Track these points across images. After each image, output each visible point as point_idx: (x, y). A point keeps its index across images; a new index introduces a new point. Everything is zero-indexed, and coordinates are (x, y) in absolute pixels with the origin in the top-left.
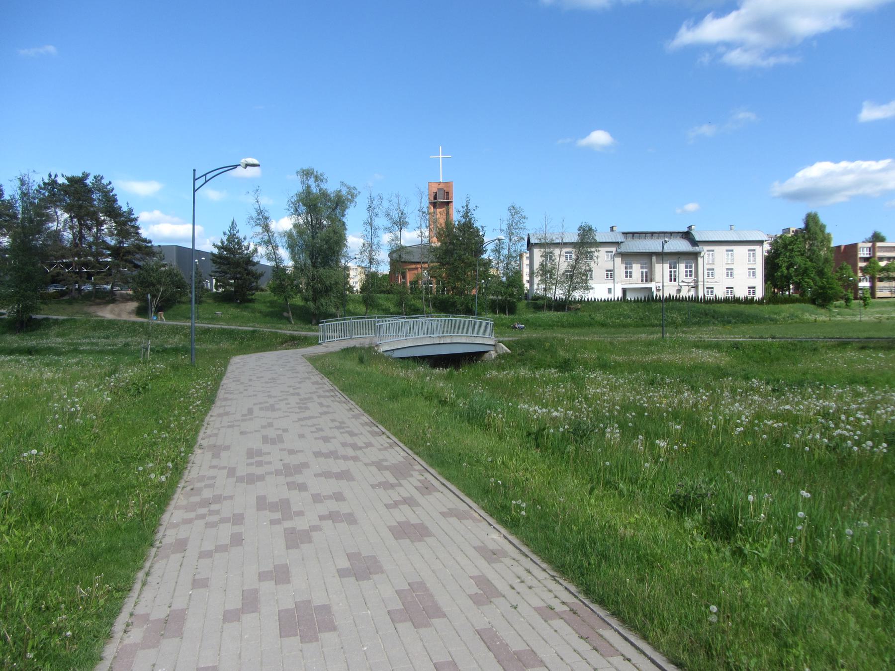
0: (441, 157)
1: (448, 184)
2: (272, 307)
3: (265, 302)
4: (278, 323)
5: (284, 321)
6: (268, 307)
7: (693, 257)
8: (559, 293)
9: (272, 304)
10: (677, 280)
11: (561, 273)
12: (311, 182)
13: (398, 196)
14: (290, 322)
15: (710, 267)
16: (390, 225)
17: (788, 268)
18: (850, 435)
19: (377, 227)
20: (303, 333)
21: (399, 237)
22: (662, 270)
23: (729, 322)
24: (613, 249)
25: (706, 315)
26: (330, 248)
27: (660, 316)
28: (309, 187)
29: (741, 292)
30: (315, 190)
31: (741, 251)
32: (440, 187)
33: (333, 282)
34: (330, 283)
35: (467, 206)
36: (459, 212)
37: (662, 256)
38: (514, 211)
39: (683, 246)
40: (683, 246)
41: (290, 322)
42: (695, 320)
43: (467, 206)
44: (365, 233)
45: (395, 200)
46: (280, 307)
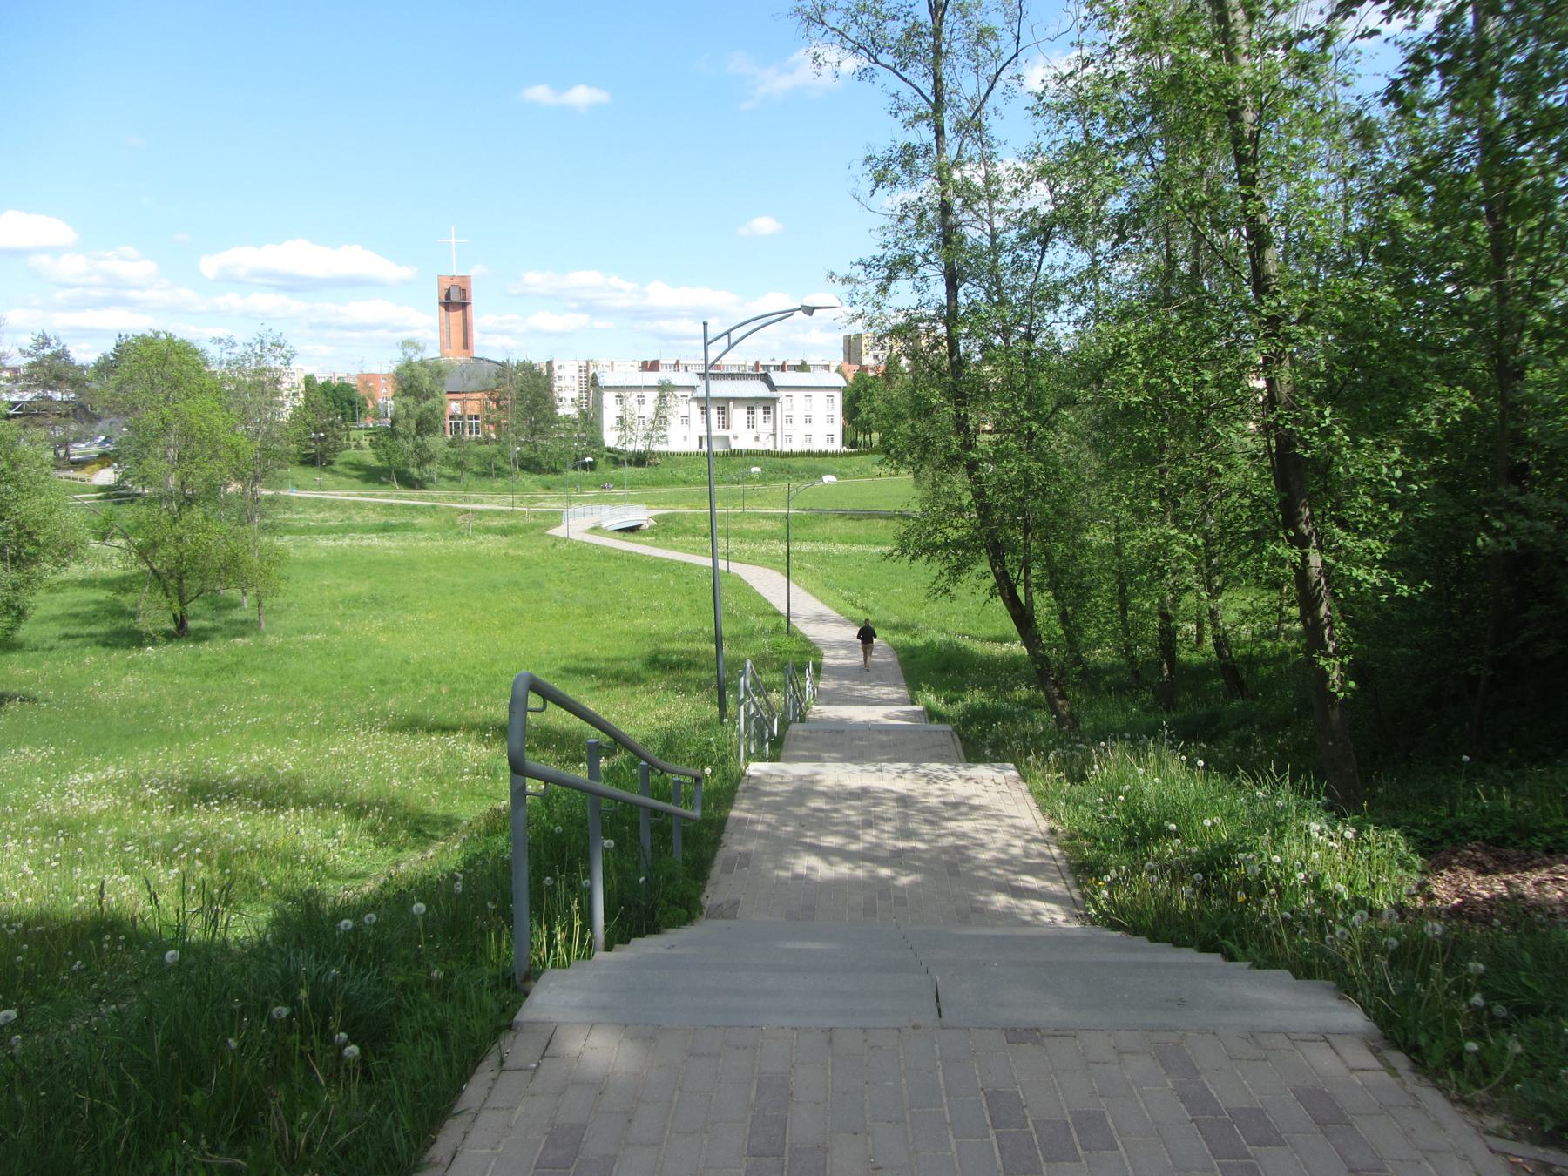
0: (453, 241)
1: (465, 279)
18: (1318, 265)
23: (803, 477)
24: (688, 393)
27: (739, 471)
39: (758, 389)
40: (758, 389)
42: (771, 475)
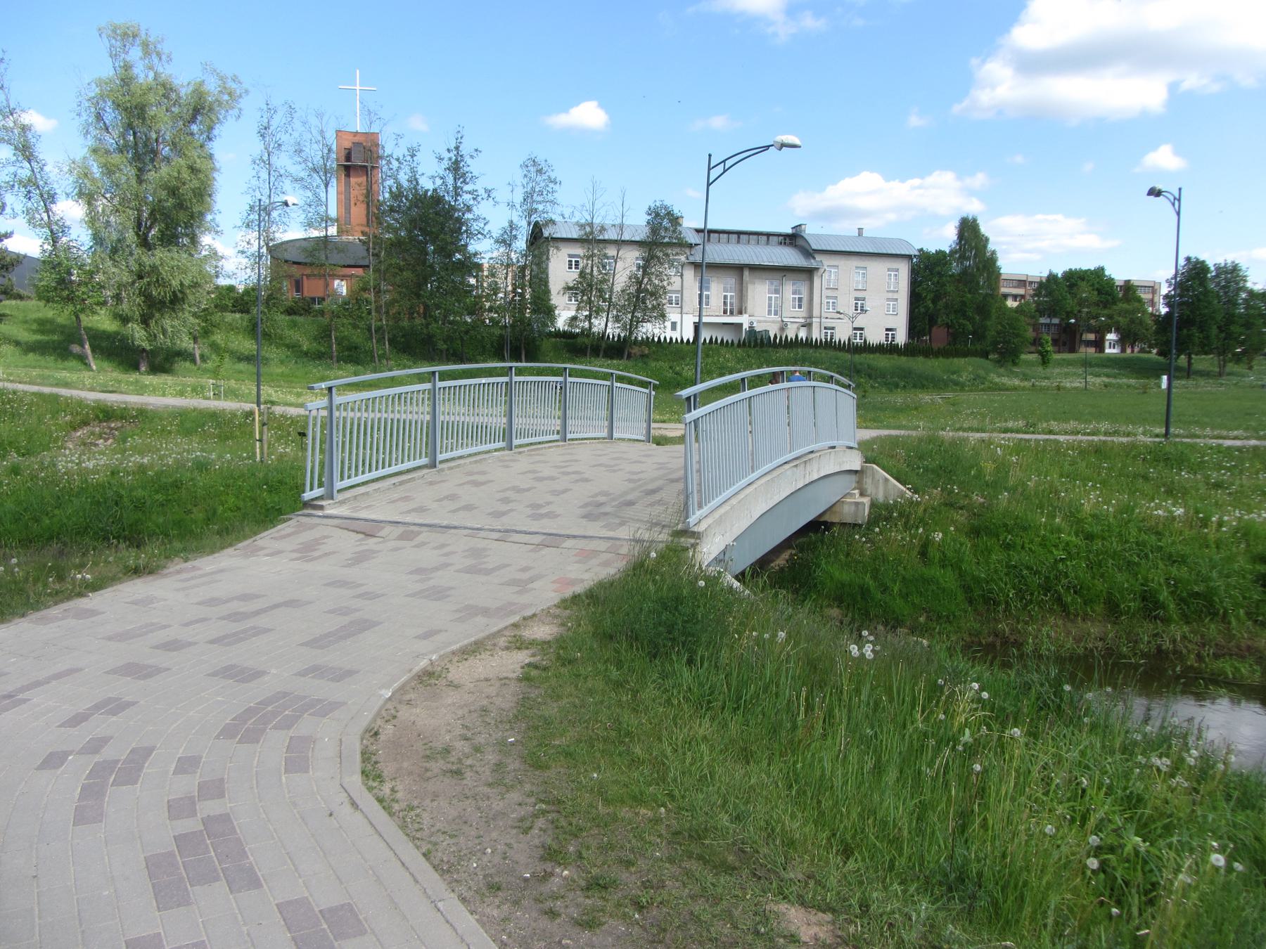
0: (358, 88)
2: (42, 332)
3: (26, 322)
4: (57, 368)
5: (73, 363)
6: (35, 332)
7: (804, 276)
8: (607, 326)
9: (44, 325)
10: (779, 313)
11: (619, 289)
12: (135, 54)
13: (320, 116)
14: (87, 366)
15: (830, 293)
16: (303, 174)
17: (934, 301)
19: (282, 172)
20: (133, 399)
21: (324, 199)
22: (760, 293)
23: (897, 386)
25: (858, 372)
26: (181, 206)
28: (127, 67)
29: (875, 337)
30: (142, 75)
31: (878, 269)
32: (357, 139)
33: (186, 283)
34: (182, 284)
35: (457, 148)
36: (442, 159)
37: (756, 269)
38: (535, 167)
39: (789, 257)
40: (789, 257)
41: (87, 366)
43: (457, 148)
44: (254, 182)
45: (314, 121)
46: (62, 332)
